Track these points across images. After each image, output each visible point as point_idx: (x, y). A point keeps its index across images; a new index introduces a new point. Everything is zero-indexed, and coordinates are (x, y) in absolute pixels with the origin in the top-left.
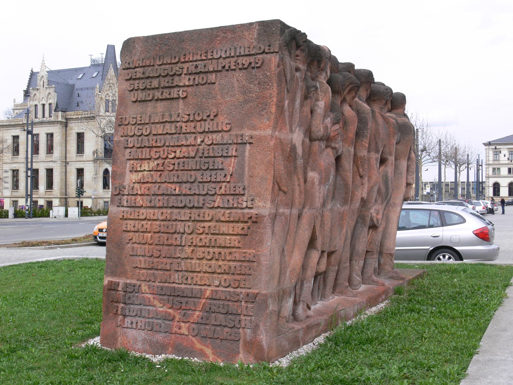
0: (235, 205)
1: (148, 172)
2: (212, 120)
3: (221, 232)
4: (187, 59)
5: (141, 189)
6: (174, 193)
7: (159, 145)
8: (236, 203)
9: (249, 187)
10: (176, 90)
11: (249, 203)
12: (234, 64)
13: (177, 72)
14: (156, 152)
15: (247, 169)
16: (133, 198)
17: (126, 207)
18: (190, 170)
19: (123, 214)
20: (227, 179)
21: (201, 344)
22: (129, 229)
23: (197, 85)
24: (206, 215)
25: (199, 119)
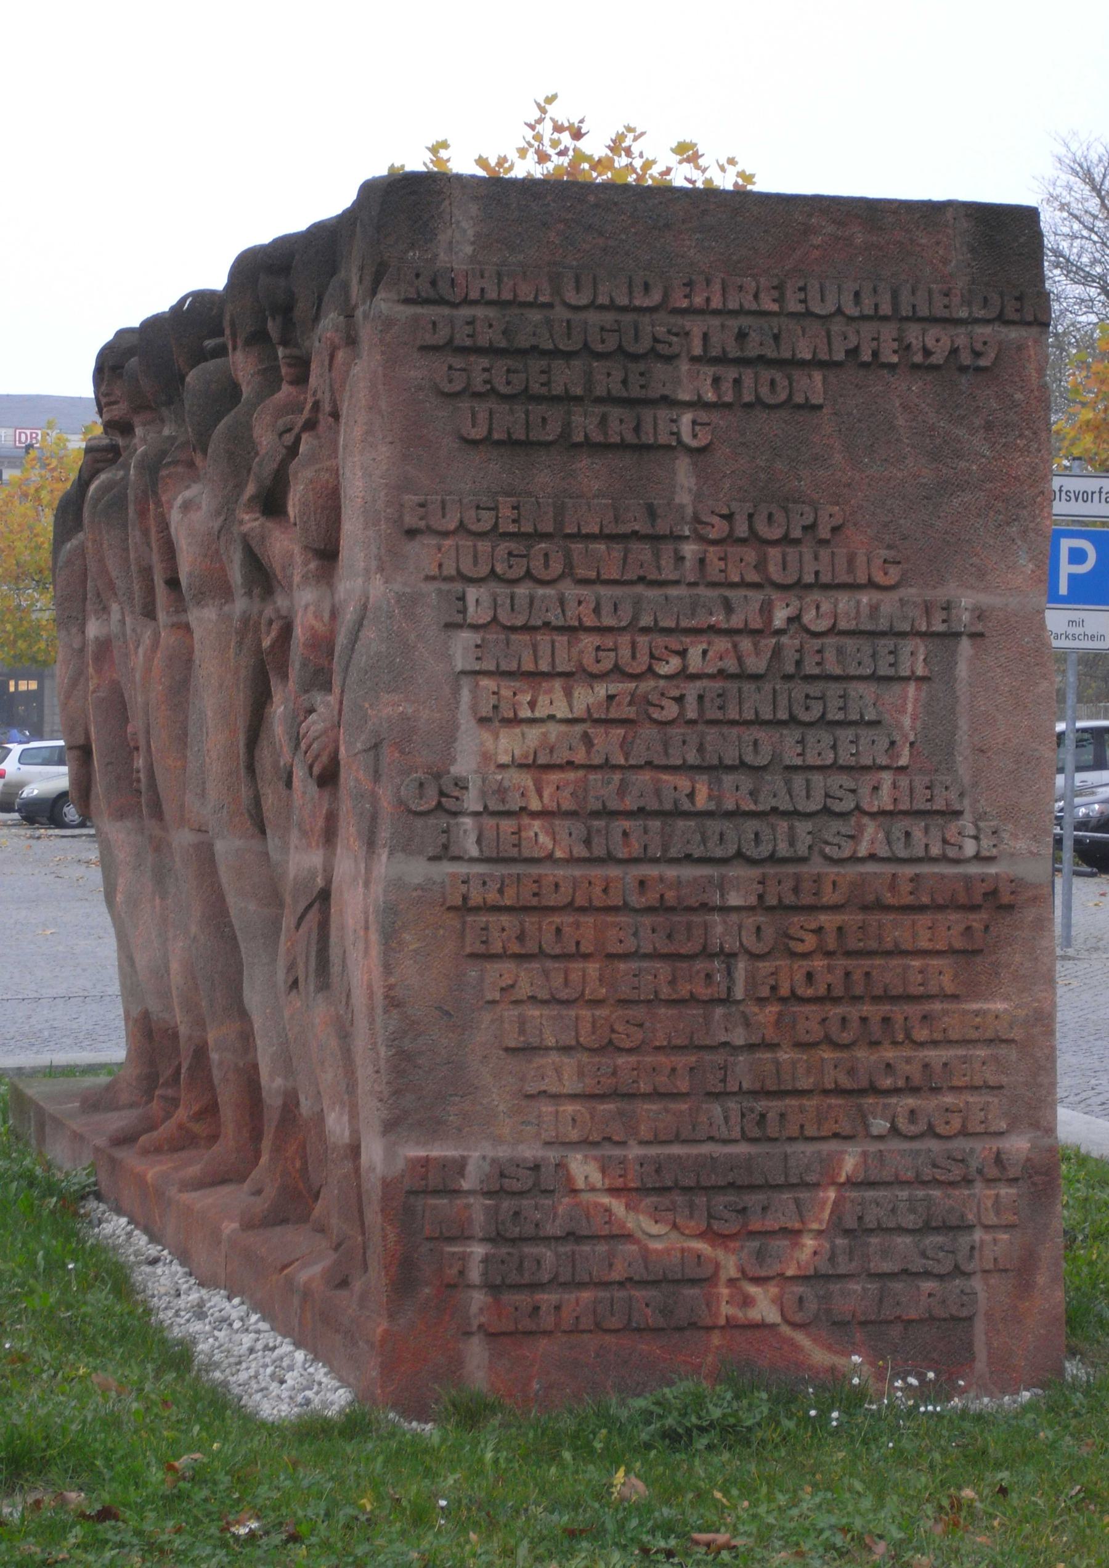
0: (935, 851)
1: (563, 728)
2: (42, 487)
3: (889, 945)
4: (698, 301)
5: (539, 792)
6: (686, 806)
7: (608, 621)
8: (939, 844)
9: (975, 785)
10: (664, 414)
11: (985, 843)
12: (895, 345)
13: (660, 347)
14: (598, 648)
15: (963, 724)
16: (508, 825)
17: (472, 860)
18: (747, 723)
19: (463, 888)
20: (899, 756)
21: (829, 1348)
22: (497, 947)
23: (749, 406)
24: (828, 888)
25: (776, 533)
